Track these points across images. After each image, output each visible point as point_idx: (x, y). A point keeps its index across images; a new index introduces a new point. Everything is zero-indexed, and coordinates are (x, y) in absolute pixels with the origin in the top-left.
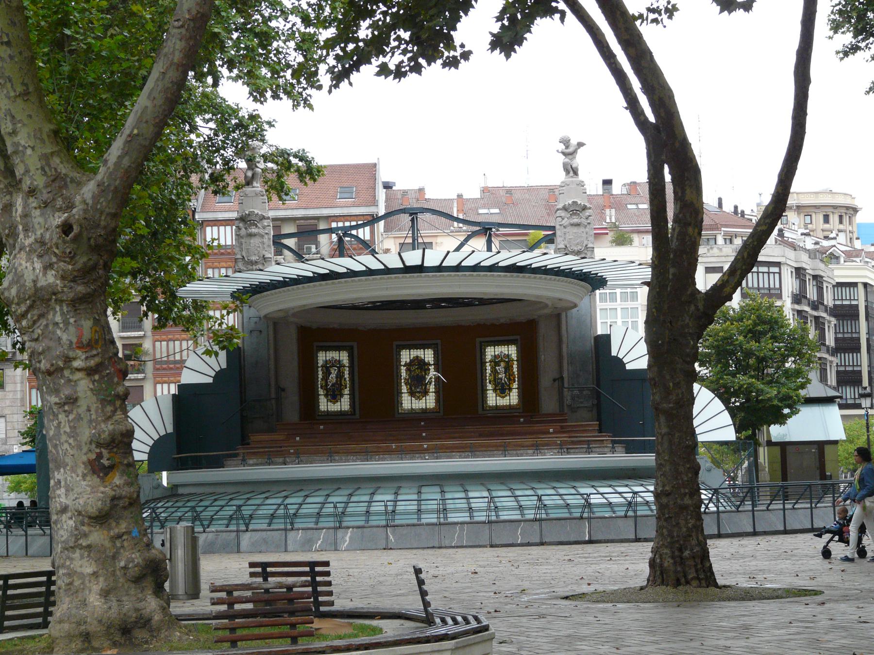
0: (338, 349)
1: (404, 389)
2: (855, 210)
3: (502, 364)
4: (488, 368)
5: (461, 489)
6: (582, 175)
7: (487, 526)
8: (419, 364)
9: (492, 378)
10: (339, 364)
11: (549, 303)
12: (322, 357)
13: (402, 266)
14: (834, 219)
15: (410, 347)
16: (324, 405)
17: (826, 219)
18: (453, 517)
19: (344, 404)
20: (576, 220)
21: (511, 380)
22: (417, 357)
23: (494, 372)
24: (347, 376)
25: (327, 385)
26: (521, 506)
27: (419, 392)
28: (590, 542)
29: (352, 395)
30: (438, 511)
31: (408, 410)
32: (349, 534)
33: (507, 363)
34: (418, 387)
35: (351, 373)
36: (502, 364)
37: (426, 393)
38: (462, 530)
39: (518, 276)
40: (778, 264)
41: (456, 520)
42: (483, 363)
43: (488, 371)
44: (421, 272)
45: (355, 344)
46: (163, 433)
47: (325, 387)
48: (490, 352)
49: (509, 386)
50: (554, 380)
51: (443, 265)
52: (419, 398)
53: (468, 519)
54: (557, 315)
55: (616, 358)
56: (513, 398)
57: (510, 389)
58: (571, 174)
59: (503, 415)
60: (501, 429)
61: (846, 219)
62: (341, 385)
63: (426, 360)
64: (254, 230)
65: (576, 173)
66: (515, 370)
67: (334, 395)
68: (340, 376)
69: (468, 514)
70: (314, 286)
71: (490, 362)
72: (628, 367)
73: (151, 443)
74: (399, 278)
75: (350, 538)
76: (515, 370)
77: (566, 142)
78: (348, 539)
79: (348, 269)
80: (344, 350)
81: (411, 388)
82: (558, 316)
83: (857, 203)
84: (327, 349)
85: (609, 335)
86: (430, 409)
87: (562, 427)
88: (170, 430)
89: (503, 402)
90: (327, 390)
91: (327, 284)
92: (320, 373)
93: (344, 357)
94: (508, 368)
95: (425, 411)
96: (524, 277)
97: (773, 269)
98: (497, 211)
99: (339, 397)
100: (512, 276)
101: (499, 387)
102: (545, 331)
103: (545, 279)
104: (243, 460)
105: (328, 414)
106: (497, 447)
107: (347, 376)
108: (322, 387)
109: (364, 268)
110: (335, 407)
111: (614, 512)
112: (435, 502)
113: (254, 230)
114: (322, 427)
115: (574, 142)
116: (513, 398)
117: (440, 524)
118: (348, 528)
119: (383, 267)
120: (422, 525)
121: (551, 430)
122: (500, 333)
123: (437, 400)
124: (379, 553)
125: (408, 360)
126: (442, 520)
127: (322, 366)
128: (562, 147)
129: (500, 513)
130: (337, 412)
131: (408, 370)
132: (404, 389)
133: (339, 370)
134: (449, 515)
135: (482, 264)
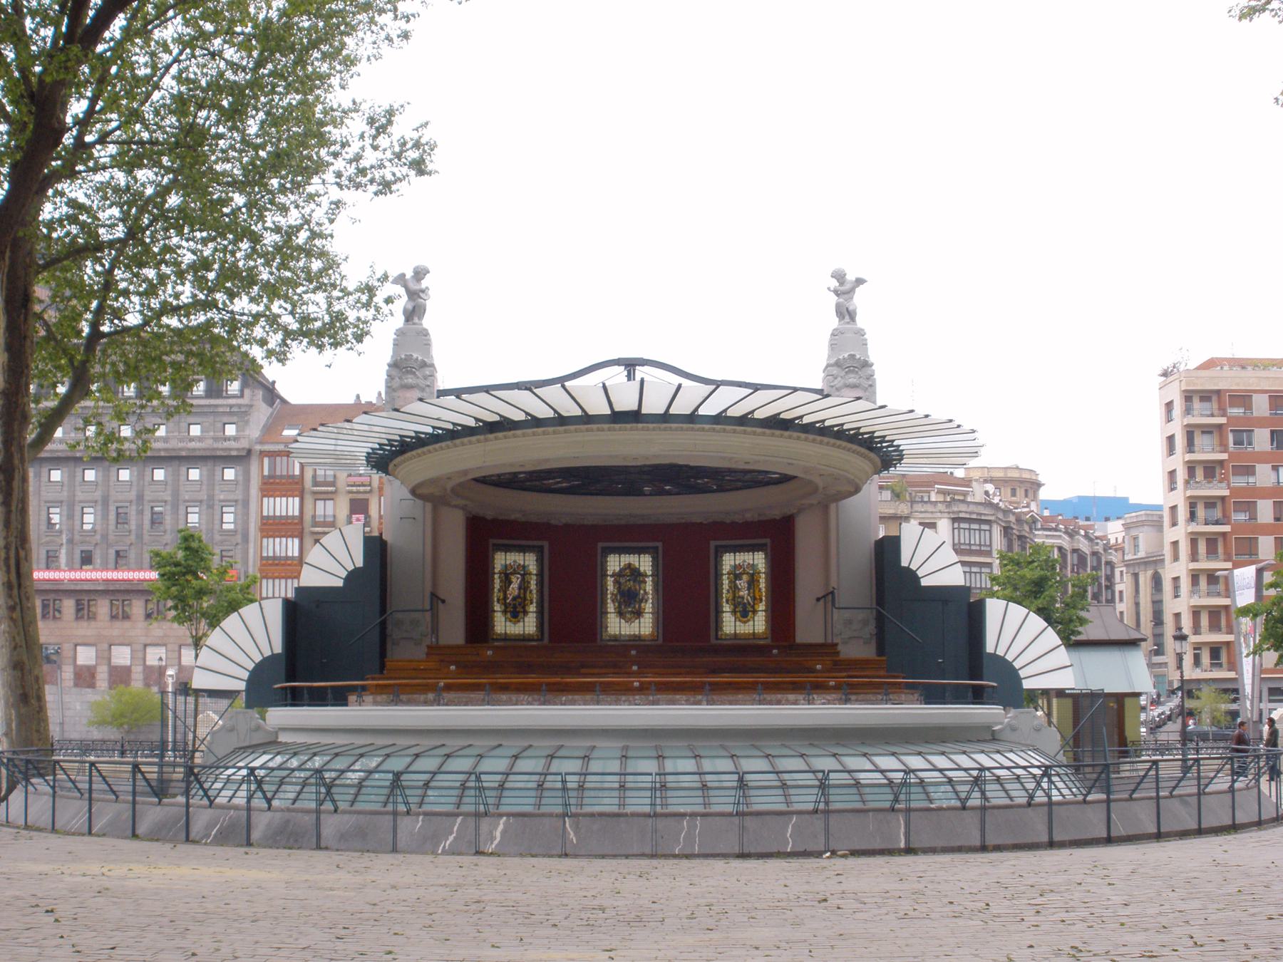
0: (523, 549)
1: (611, 607)
2: (1038, 485)
3: (745, 577)
6: (861, 322)
7: (736, 820)
8: (632, 574)
9: (730, 596)
11: (820, 482)
12: (501, 560)
14: (1020, 492)
16: (501, 625)
17: (1014, 493)
18: (678, 803)
19: (529, 625)
20: (852, 379)
22: (630, 565)
23: (734, 588)
25: (505, 598)
29: (540, 613)
30: (653, 789)
32: (501, 827)
33: (752, 575)
34: (629, 602)
35: (540, 583)
36: (745, 577)
37: (639, 614)
40: (988, 522)
41: (682, 809)
42: (718, 575)
45: (546, 544)
46: (267, 653)
48: (729, 561)
50: (818, 600)
51: (671, 411)
55: (908, 569)
56: (759, 624)
57: (755, 612)
58: (847, 318)
59: (743, 648)
62: (525, 599)
63: (642, 569)
64: (410, 380)
65: (853, 318)
67: (516, 612)
68: (524, 587)
72: (924, 582)
75: (504, 833)
76: (762, 585)
77: (839, 276)
78: (498, 834)
79: (527, 414)
81: (620, 607)
84: (507, 549)
88: (278, 649)
89: (744, 629)
90: (505, 604)
93: (530, 561)
94: (753, 582)
95: (637, 638)
97: (984, 527)
105: (506, 638)
109: (551, 414)
110: (515, 629)
112: (649, 778)
113: (410, 380)
115: (851, 277)
117: (656, 815)
118: (501, 815)
119: (579, 413)
120: (626, 815)
122: (743, 534)
123: (656, 623)
125: (617, 569)
126: (659, 809)
128: (834, 283)
131: (616, 582)
133: (523, 579)
135: (729, 413)
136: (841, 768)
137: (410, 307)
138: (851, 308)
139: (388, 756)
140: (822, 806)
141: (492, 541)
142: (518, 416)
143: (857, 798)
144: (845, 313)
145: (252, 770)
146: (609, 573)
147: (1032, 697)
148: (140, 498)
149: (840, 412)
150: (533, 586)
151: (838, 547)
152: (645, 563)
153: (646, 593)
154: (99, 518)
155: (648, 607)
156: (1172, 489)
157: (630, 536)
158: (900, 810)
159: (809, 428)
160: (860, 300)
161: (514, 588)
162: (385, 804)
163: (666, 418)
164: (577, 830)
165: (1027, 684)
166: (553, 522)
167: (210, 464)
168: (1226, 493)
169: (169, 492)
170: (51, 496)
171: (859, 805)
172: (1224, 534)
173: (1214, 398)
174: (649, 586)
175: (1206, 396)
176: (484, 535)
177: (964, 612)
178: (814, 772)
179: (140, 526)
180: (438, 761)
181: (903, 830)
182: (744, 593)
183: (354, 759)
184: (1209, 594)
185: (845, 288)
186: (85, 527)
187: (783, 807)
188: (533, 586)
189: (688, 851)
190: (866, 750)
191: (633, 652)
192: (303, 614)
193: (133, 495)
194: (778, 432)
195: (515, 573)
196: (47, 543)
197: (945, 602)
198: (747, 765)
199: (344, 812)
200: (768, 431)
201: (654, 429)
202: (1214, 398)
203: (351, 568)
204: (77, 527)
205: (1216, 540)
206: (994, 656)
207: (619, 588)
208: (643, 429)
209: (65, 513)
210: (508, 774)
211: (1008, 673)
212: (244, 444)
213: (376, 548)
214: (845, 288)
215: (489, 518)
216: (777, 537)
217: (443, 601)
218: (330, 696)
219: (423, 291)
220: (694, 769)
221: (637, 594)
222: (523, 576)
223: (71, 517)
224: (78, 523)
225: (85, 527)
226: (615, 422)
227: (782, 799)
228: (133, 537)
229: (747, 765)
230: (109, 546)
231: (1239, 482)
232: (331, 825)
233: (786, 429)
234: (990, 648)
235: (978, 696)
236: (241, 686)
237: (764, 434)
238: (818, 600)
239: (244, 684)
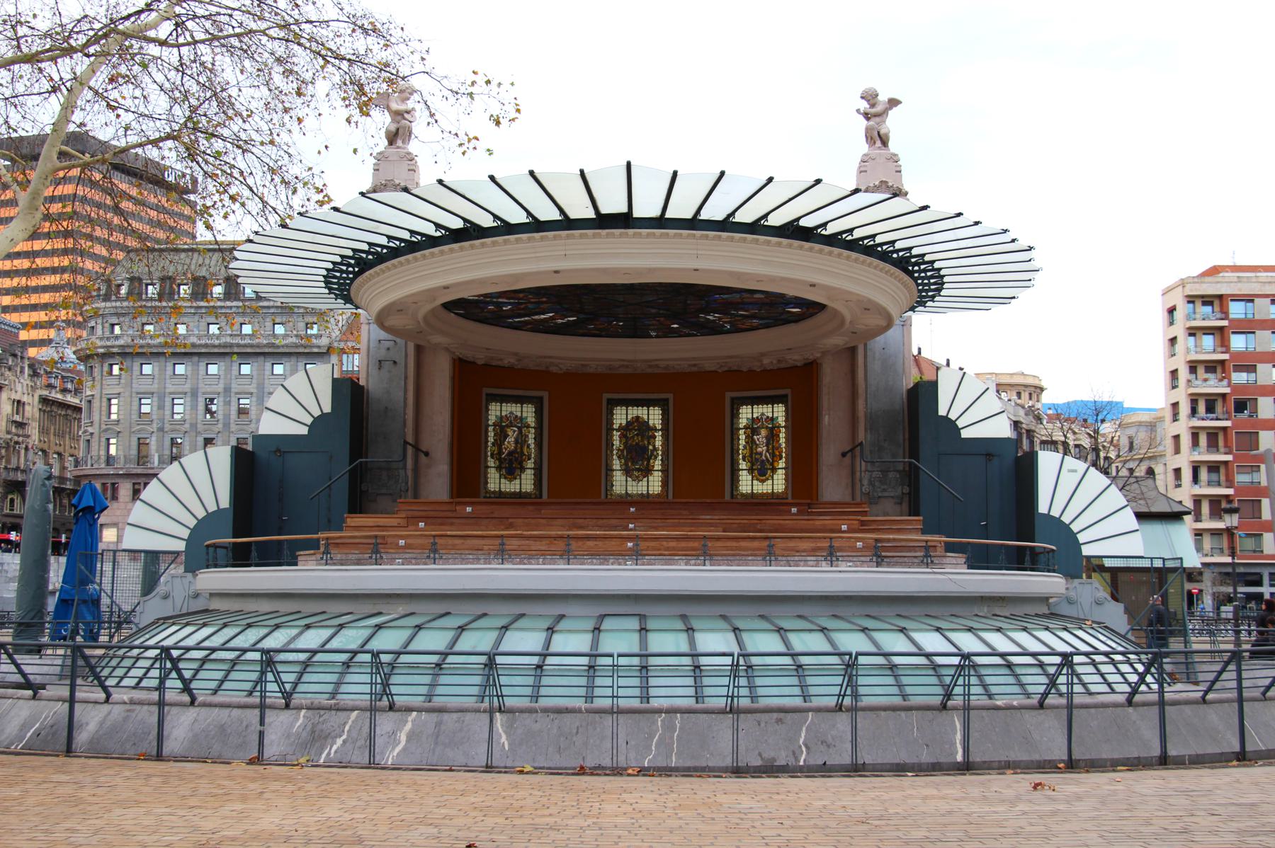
1: (616, 464)
2: (1042, 389)
3: (763, 432)
4: (742, 437)
5: (680, 625)
6: (893, 146)
9: (747, 452)
10: (520, 423)
12: (495, 411)
13: (591, 214)
21: (776, 457)
23: (751, 442)
24: (531, 441)
25: (500, 453)
26: (800, 666)
27: (638, 470)
28: (966, 767)
31: (621, 496)
32: (409, 726)
33: (772, 429)
34: (637, 460)
36: (763, 432)
37: (647, 471)
38: (670, 728)
39: (801, 248)
42: (734, 431)
43: (742, 442)
44: (627, 227)
45: (545, 395)
46: (212, 508)
47: (497, 455)
48: (746, 414)
49: (772, 464)
50: (844, 455)
51: (668, 215)
52: (638, 479)
53: (690, 702)
54: (859, 339)
55: (946, 418)
56: (778, 483)
57: (774, 470)
58: (879, 143)
60: (761, 526)
61: (1034, 396)
63: (651, 422)
65: (884, 142)
66: (782, 441)
69: (690, 681)
70: (442, 253)
71: (745, 428)
72: (965, 434)
73: (192, 523)
74: (586, 236)
76: (782, 441)
77: (870, 97)
79: (496, 217)
80: (529, 403)
81: (626, 464)
82: (853, 350)
83: (1044, 384)
84: (503, 399)
86: (653, 495)
87: (863, 523)
88: (225, 502)
90: (500, 460)
91: (462, 249)
92: (491, 434)
93: (528, 413)
96: (811, 249)
99: (518, 472)
100: (790, 246)
101: (757, 466)
102: (831, 377)
103: (848, 258)
104: (327, 552)
106: (754, 553)
107: (531, 441)
108: (492, 456)
111: (990, 696)
114: (469, 509)
115: (883, 98)
116: (778, 483)
118: (409, 710)
121: (844, 527)
122: (761, 384)
123: (665, 483)
124: (461, 780)
125: (624, 422)
127: (494, 425)
128: (864, 105)
129: (759, 681)
130: (514, 493)
132: (616, 464)
134: (652, 682)
136: (873, 649)
137: (393, 128)
138: (882, 132)
139: (379, 627)
140: (847, 701)
142: (486, 221)
143: (895, 690)
144: (878, 138)
145: (166, 650)
147: (1095, 566)
148: (227, 390)
149: (869, 218)
151: (866, 379)
152: (654, 417)
153: (655, 449)
154: (188, 408)
155: (658, 464)
156: (1174, 388)
157: (638, 386)
158: (955, 708)
159: (834, 240)
160: (893, 123)
161: (511, 439)
162: (250, 693)
163: (661, 222)
164: (509, 729)
165: (1087, 551)
166: (554, 369)
167: (293, 359)
168: (1227, 390)
169: (254, 385)
170: (143, 389)
171: (897, 700)
172: (1224, 429)
173: (1216, 303)
174: (658, 442)
175: (1207, 300)
176: (475, 382)
177: (1013, 466)
178: (840, 654)
179: (227, 416)
180: (404, 635)
181: (959, 737)
184: (1210, 484)
185: (876, 111)
186: (176, 417)
187: (798, 702)
189: (661, 763)
190: (903, 623)
192: (251, 466)
193: (220, 388)
194: (796, 243)
195: (511, 425)
196: (139, 431)
197: (989, 456)
198: (800, 642)
199: (204, 705)
202: (1216, 303)
204: (168, 417)
205: (1216, 434)
206: (1048, 516)
207: (625, 444)
209: (155, 404)
210: (447, 654)
211: (1064, 534)
212: (324, 341)
213: (349, 392)
214: (876, 111)
215: (480, 362)
216: (797, 384)
218: (254, 554)
219: (408, 112)
220: (685, 648)
221: (645, 449)
223: (161, 407)
224: (168, 412)
225: (176, 417)
227: (797, 691)
228: (220, 426)
229: (800, 642)
230: (198, 433)
231: (1240, 378)
232: (182, 725)
233: (807, 240)
234: (1042, 508)
235: (1022, 560)
236: (180, 546)
238: (844, 455)
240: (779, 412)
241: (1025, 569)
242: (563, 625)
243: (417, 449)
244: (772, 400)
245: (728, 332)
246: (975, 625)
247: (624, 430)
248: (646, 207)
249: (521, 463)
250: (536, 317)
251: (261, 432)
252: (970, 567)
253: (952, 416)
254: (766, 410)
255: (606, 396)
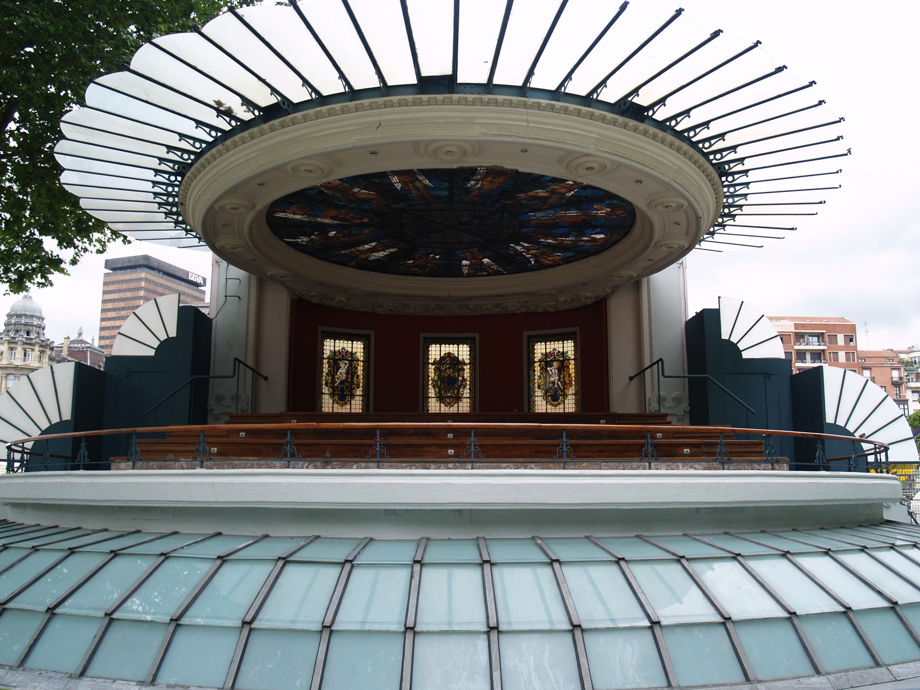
1: (432, 392)
9: (542, 381)
10: (350, 357)
15: (441, 341)
25: (333, 382)
27: (450, 397)
29: (366, 396)
33: (562, 362)
35: (366, 369)
36: (555, 364)
37: (458, 398)
42: (531, 362)
47: (331, 384)
48: (330, 346)
49: (563, 391)
50: (631, 379)
51: (495, 82)
55: (728, 342)
62: (352, 383)
63: (460, 358)
81: (440, 392)
84: (336, 337)
85: (719, 310)
90: (333, 387)
92: (326, 366)
93: (358, 348)
94: (563, 368)
98: (602, 236)
99: (348, 398)
108: (326, 384)
122: (552, 325)
125: (438, 358)
133: (351, 365)
141: (321, 328)
146: (431, 361)
150: (360, 369)
152: (463, 352)
153: (464, 380)
155: (466, 392)
161: (343, 370)
163: (489, 87)
174: (467, 374)
182: (555, 378)
183: (60, 555)
188: (360, 369)
191: (450, 436)
197: (767, 375)
200: (620, 119)
201: (473, 103)
203: (163, 337)
207: (439, 378)
208: (458, 103)
213: (193, 320)
215: (315, 301)
216: (588, 323)
217: (266, 379)
221: (456, 380)
222: (351, 362)
226: (422, 92)
237: (614, 123)
239: (59, 420)
240: (568, 347)
241: (817, 469)
242: (370, 555)
243: (256, 373)
244: (562, 338)
245: (532, 269)
246: (898, 543)
247: (439, 363)
248: (472, 72)
249: (351, 391)
250: (361, 248)
251: (113, 354)
252: (791, 468)
253: (734, 339)
254: (557, 346)
255: (423, 335)
